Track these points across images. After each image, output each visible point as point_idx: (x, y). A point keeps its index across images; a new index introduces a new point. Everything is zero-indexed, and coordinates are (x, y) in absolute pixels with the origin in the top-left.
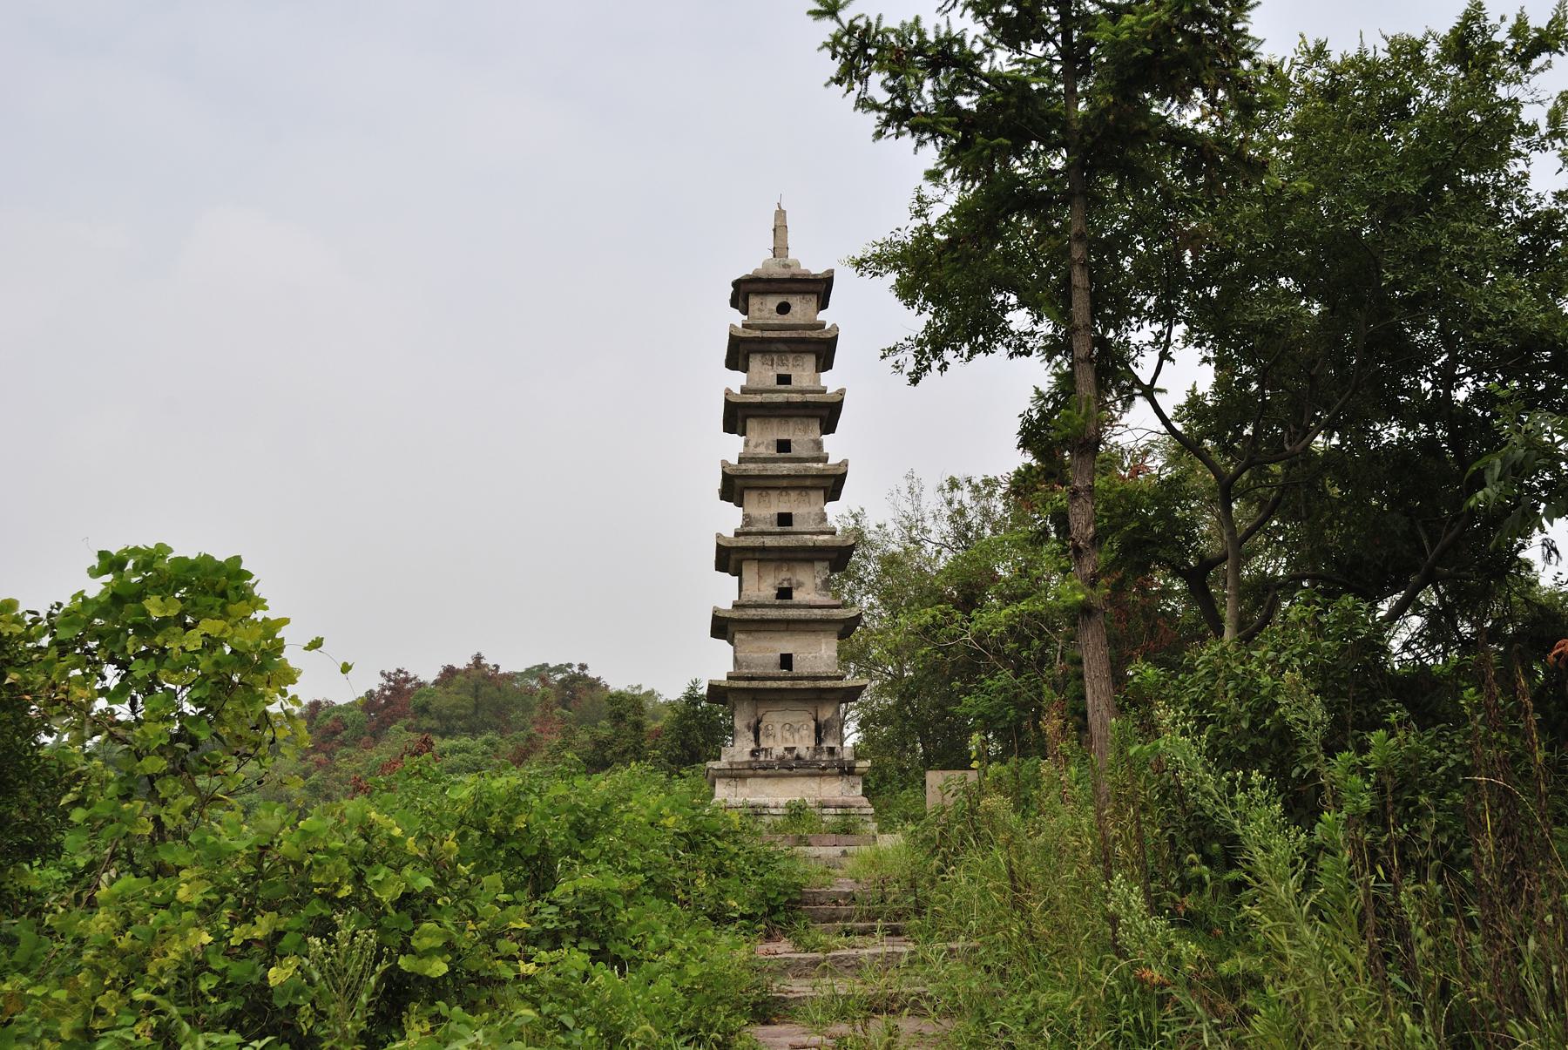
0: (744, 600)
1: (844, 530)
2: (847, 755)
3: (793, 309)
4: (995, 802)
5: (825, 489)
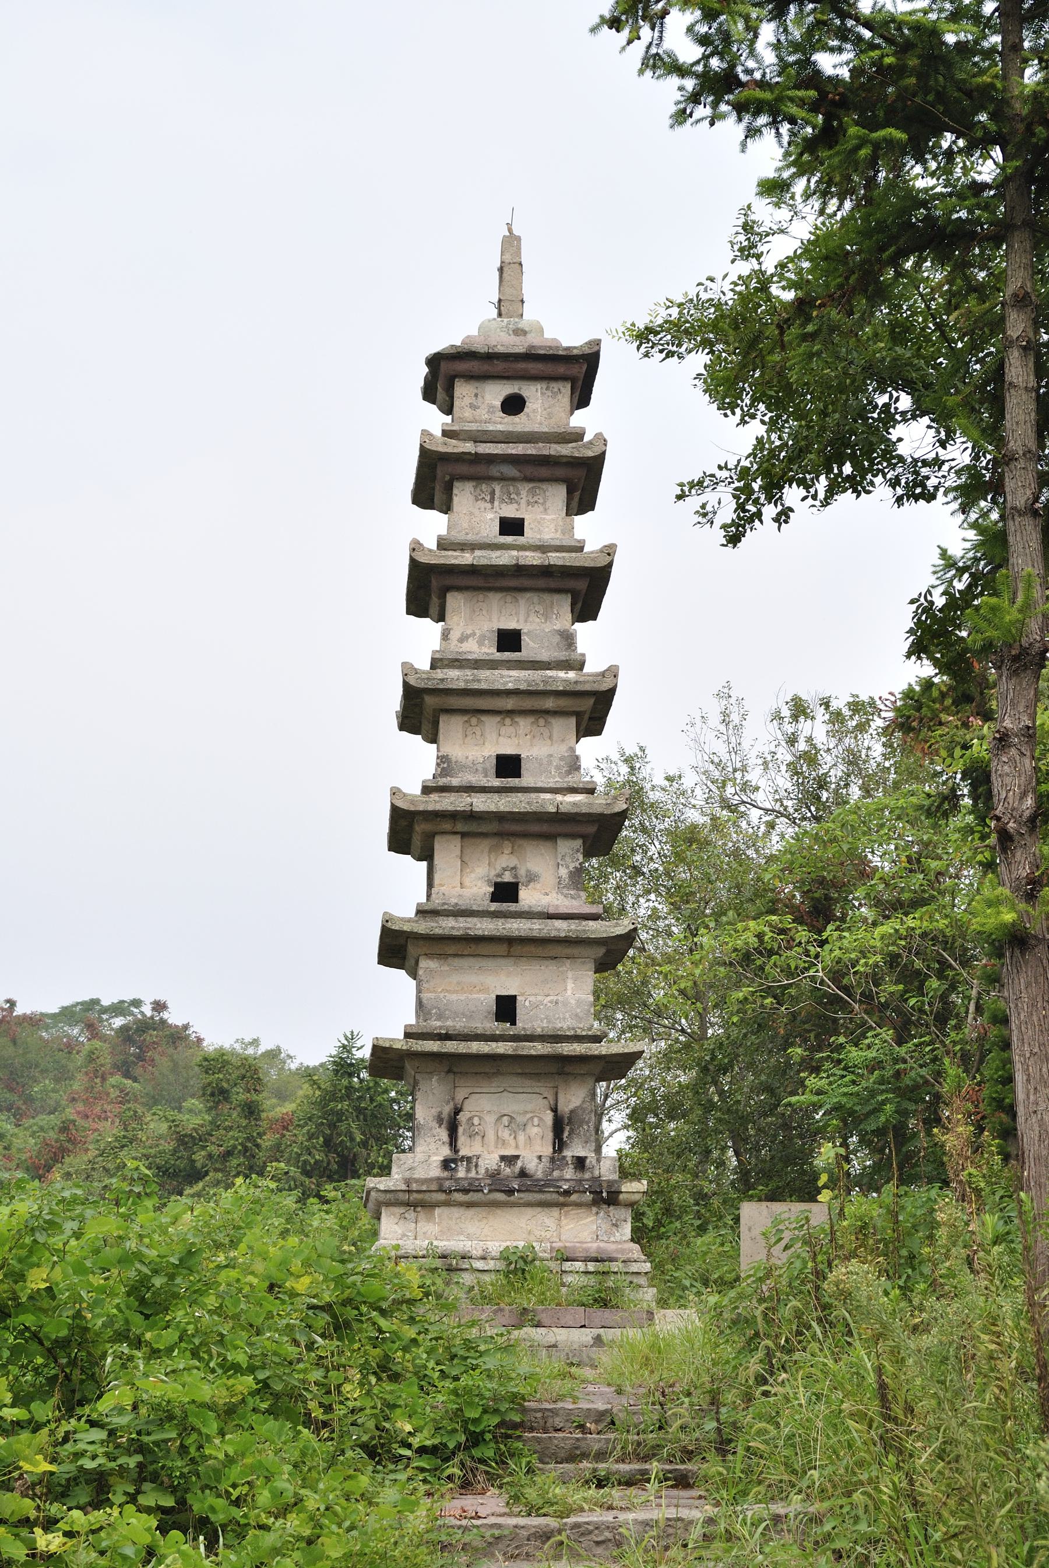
0: (437, 902)
1: (609, 783)
2: (607, 1171)
3: (529, 407)
4: (857, 1275)
5: (578, 715)
